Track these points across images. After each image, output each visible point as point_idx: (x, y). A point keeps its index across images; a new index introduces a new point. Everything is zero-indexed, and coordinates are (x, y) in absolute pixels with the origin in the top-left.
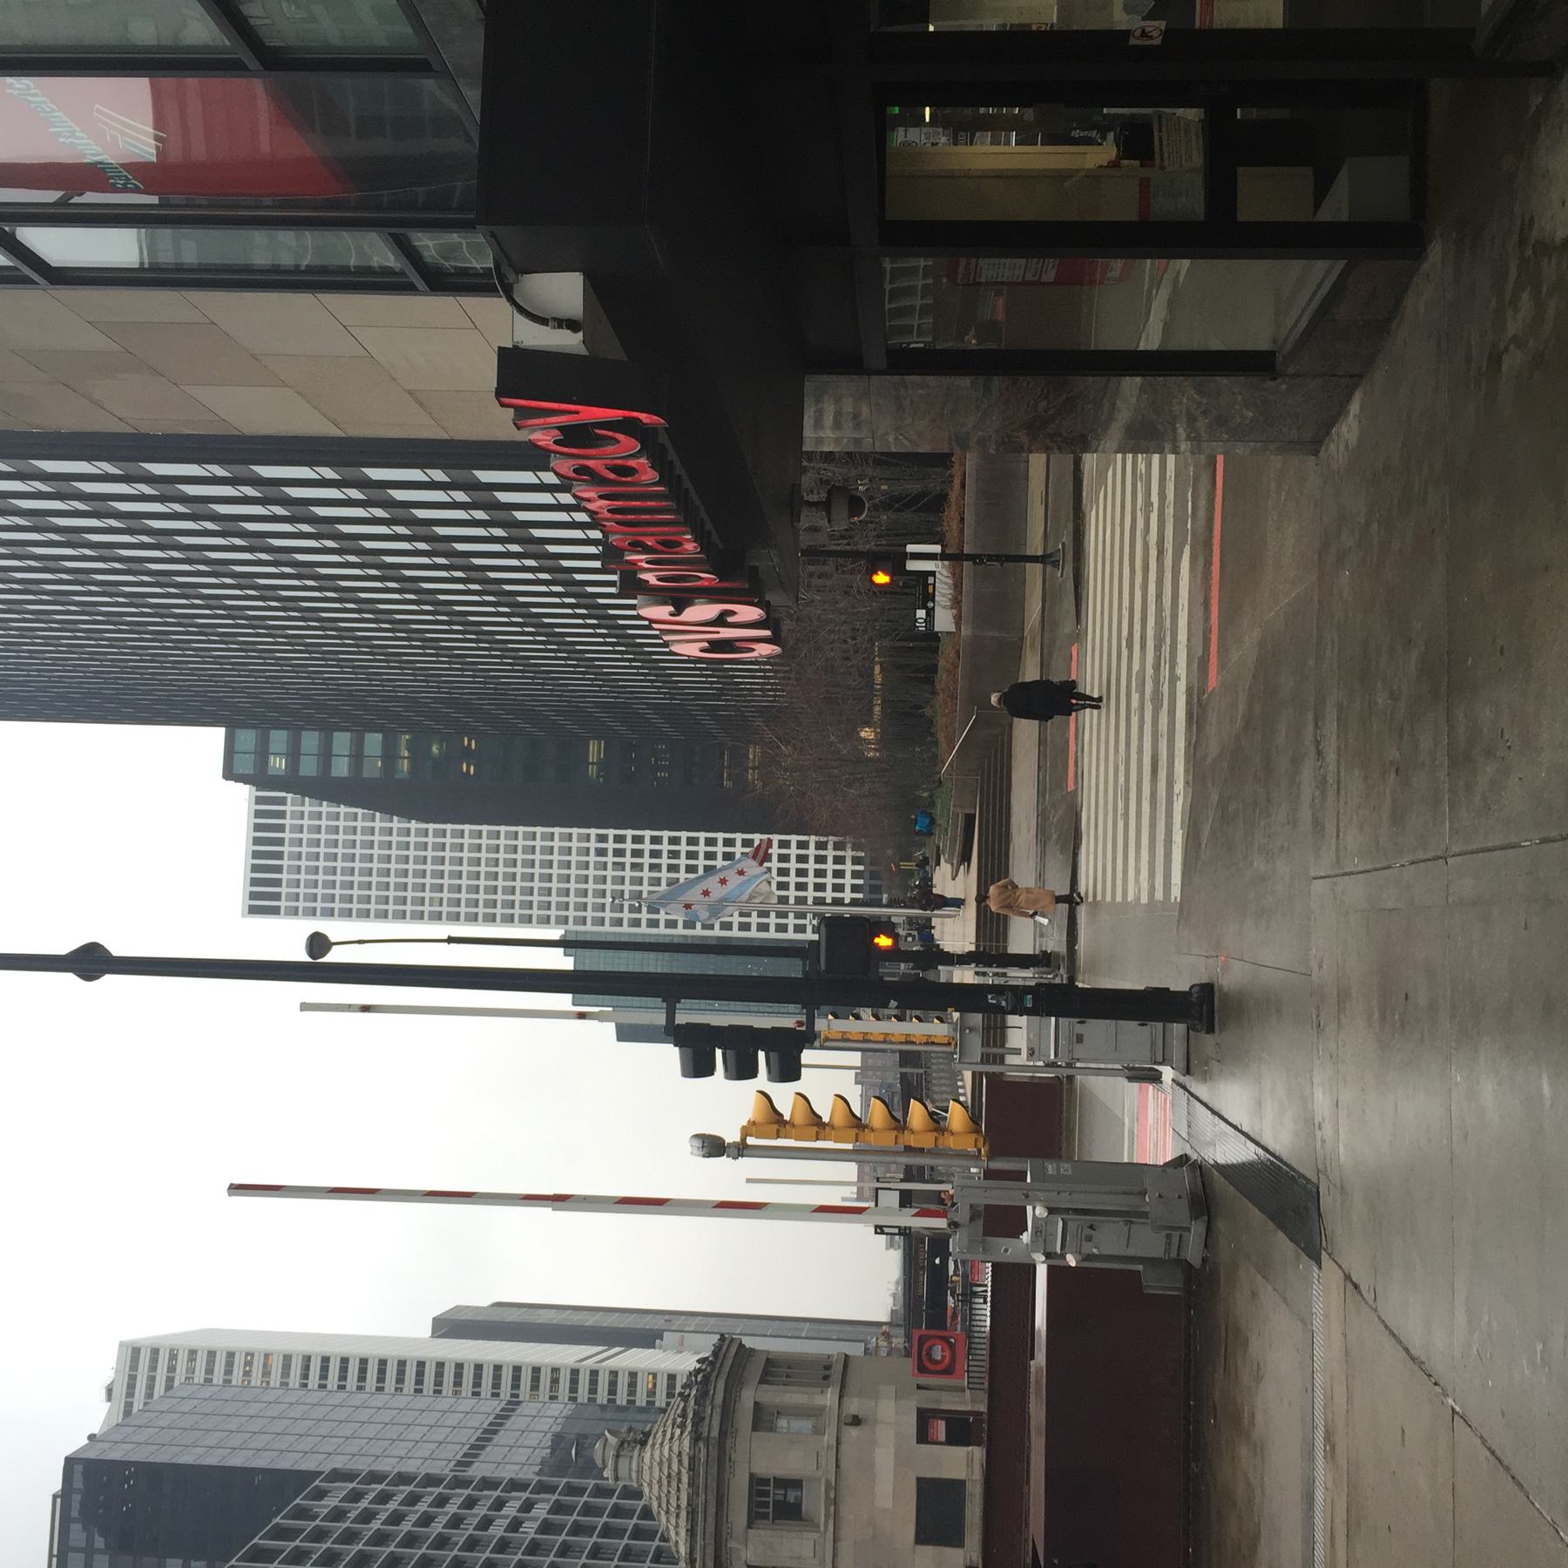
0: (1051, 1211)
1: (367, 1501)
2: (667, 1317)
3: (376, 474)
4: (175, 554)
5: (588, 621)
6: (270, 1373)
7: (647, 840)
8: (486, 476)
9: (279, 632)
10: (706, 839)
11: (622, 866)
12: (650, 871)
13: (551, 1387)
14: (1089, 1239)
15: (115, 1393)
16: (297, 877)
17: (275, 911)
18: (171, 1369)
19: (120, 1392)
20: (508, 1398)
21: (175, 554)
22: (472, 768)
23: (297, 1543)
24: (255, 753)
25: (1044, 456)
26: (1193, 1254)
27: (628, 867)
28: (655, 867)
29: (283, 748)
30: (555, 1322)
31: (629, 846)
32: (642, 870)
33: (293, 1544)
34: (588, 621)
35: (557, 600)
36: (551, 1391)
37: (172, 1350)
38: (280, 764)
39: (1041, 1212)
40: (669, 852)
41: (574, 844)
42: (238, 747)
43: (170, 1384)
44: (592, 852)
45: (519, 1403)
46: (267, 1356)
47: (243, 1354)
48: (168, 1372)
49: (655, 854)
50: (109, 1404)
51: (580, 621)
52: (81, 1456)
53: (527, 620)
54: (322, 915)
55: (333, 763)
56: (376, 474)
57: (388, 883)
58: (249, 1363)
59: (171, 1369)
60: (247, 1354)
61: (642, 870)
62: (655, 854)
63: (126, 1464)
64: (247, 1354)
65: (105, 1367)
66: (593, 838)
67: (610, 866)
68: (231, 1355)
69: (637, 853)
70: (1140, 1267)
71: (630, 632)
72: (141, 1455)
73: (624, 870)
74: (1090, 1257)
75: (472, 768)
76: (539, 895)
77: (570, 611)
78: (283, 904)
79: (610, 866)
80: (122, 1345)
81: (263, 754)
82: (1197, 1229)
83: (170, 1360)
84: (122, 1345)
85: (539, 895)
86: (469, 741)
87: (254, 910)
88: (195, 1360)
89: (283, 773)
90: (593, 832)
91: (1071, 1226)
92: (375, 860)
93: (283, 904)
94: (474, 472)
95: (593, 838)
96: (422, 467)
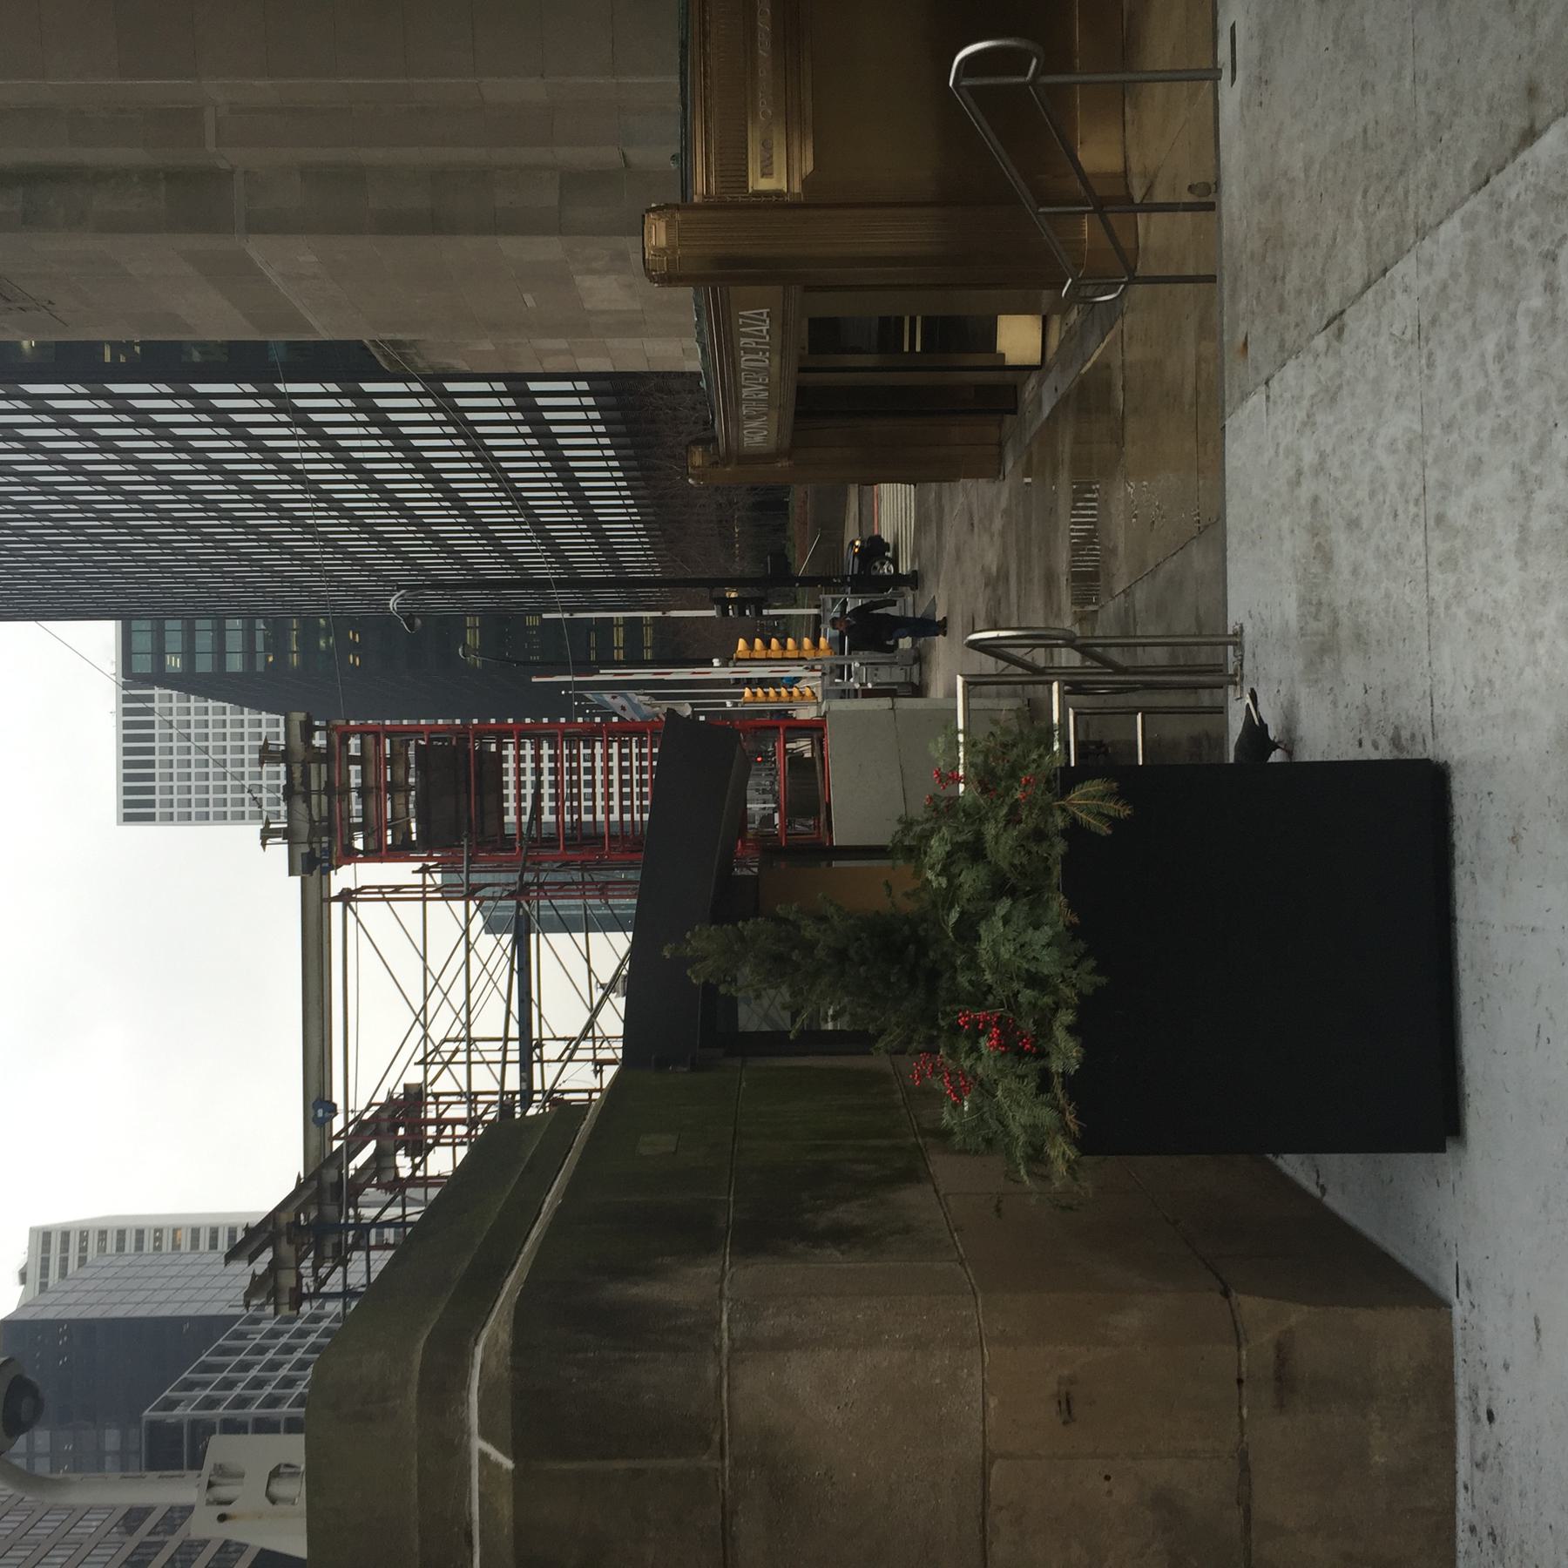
0: (861, 664)
1: (301, 1321)
3: (32, 389)
4: (12, 479)
5: (418, 535)
6: (179, 1246)
8: (368, 387)
9: (51, 565)
14: (876, 675)
15: (29, 1276)
16: (188, 770)
17: (150, 818)
18: (83, 1249)
19: (35, 1274)
21: (12, 479)
22: (358, 660)
23: (225, 1374)
24: (212, 630)
25: (149, 629)
26: (916, 680)
29: (178, 647)
33: (238, 1359)
34: (418, 535)
35: (436, 504)
37: (81, 1233)
38: (171, 660)
39: (857, 664)
42: (135, 648)
43: (82, 1261)
46: (175, 1231)
47: (152, 1232)
48: (80, 1251)
50: (23, 1287)
51: (453, 520)
52: (15, 1318)
53: (372, 536)
54: (197, 819)
55: (227, 660)
56: (32, 389)
57: (225, 813)
58: (158, 1239)
59: (83, 1249)
60: (156, 1231)
63: (60, 1322)
64: (156, 1231)
65: (18, 1252)
68: (140, 1233)
70: (895, 687)
71: (497, 535)
72: (73, 1314)
74: (878, 684)
75: (358, 660)
77: (403, 528)
78: (157, 810)
80: (32, 1230)
81: (159, 654)
82: (916, 668)
83: (81, 1241)
84: (32, 1230)
86: (354, 636)
87: (128, 818)
88: (105, 1239)
89: (180, 671)
91: (869, 670)
92: (193, 804)
93: (157, 810)
94: (361, 384)
96: (236, 382)
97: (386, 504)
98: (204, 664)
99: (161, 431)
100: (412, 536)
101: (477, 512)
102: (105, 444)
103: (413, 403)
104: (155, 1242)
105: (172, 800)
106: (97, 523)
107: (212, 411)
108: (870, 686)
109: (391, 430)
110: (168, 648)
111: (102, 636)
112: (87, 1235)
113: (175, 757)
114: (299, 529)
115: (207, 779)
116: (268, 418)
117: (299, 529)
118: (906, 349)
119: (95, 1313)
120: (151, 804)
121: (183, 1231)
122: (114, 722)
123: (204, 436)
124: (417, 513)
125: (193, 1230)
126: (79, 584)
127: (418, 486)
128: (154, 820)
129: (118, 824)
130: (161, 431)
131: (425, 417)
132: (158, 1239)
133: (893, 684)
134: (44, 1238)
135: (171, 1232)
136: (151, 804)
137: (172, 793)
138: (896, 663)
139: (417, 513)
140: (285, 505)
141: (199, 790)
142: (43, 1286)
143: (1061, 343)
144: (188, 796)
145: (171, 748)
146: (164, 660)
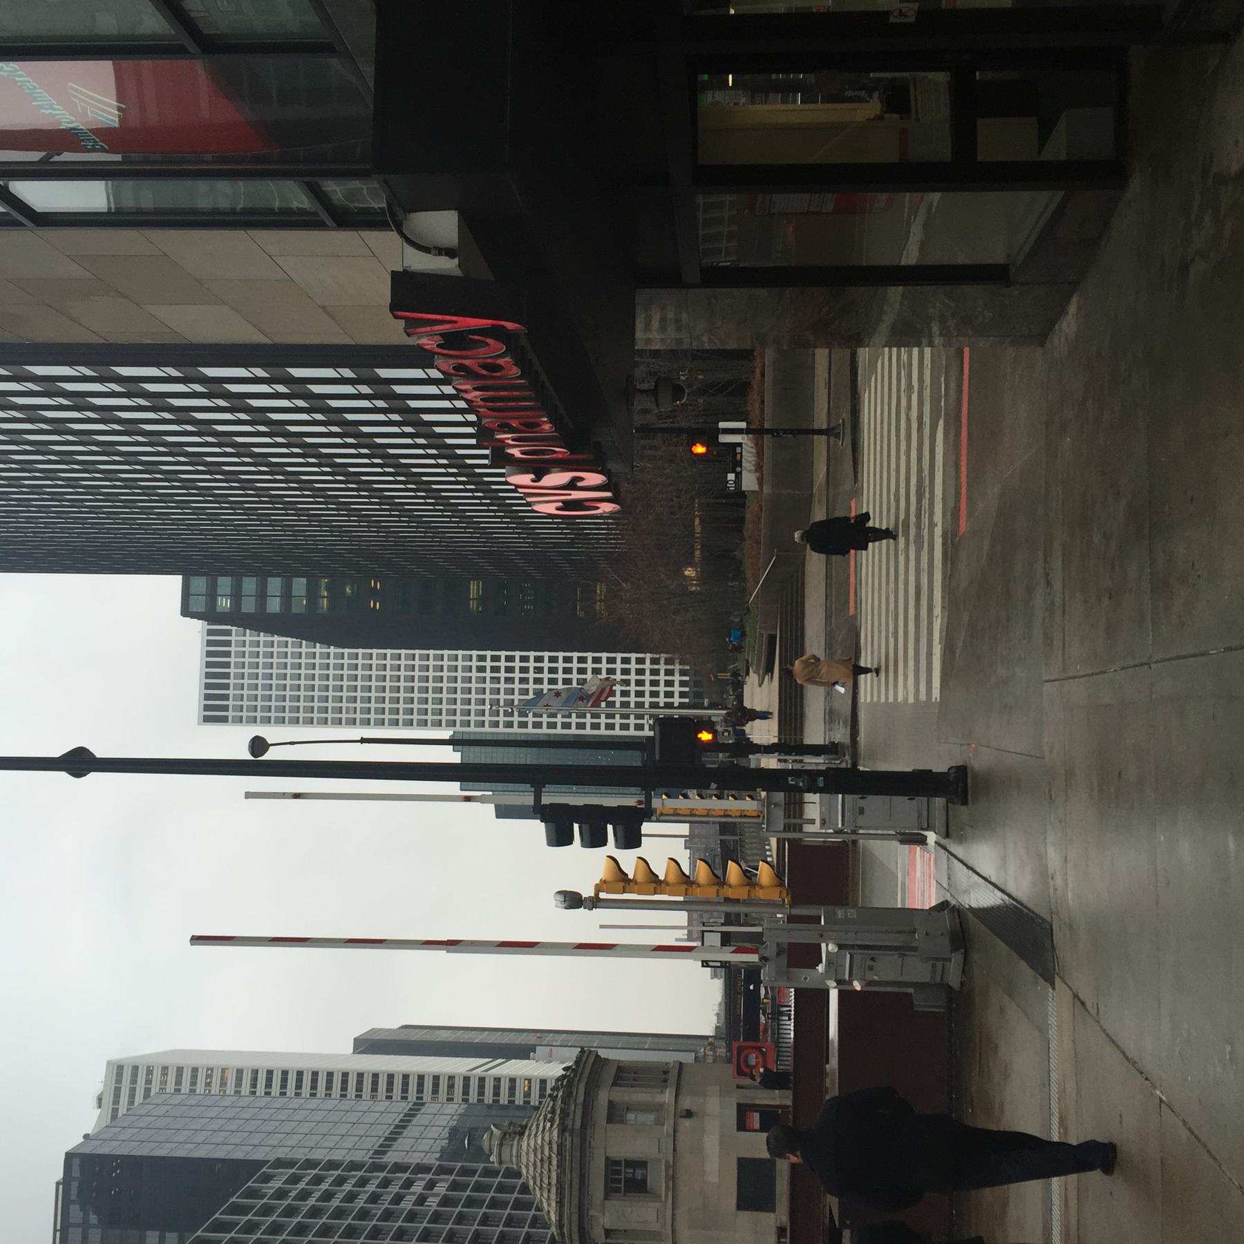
0: (841, 947)
2: (538, 1035)
5: (468, 487)
6: (226, 1084)
7: (532, 659)
10: (637, 658)
11: (498, 680)
12: (534, 684)
13: (448, 1091)
14: (871, 968)
17: (224, 720)
20: (414, 1099)
27: (502, 680)
28: (509, 680)
30: (450, 1040)
31: (503, 664)
32: (513, 683)
33: (246, 1218)
36: (448, 1094)
37: (148, 1067)
40: (535, 668)
41: (446, 663)
44: (474, 669)
45: (423, 1104)
46: (223, 1070)
48: (146, 1084)
49: (524, 670)
50: (100, 1110)
58: (209, 1076)
60: (208, 1069)
61: (513, 683)
62: (524, 670)
63: (116, 1157)
64: (208, 1069)
65: (96, 1081)
66: (474, 658)
67: (488, 680)
69: (509, 670)
70: (911, 990)
72: (124, 1150)
73: (499, 683)
74: (871, 983)
76: (433, 704)
78: (230, 714)
79: (488, 680)
82: (957, 958)
83: (148, 1074)
84: (109, 1063)
85: (433, 704)
87: (207, 719)
90: (475, 653)
91: (857, 958)
93: (230, 714)
95: (474, 658)
97: (445, 461)
98: (249, 606)
99: (258, 416)
100: (462, 487)
101: (485, 479)
102: (203, 428)
103: (432, 390)
104: (206, 1079)
105: (242, 706)
106: (225, 485)
107: (309, 396)
108: (857, 986)
109: (412, 417)
110: (219, 591)
111: (175, 581)
112: (152, 1070)
113: (275, 660)
114: (354, 486)
115: (271, 689)
116: (285, 403)
117: (354, 486)
118: (722, 425)
119: (144, 1151)
120: (226, 708)
121: (230, 1070)
122: (200, 641)
123: (298, 419)
124: (477, 471)
125: (238, 1070)
126: (213, 525)
127: (432, 461)
128: (227, 721)
129: (198, 724)
130: (258, 416)
131: (446, 404)
132: (209, 1076)
133: (906, 984)
134: (118, 1070)
135: (220, 1071)
136: (226, 708)
137: (242, 700)
138: (915, 949)
139: (477, 471)
140: (352, 470)
141: (293, 677)
142: (114, 1117)
143: (877, 361)
144: (255, 703)
145: (244, 663)
146: (216, 600)
